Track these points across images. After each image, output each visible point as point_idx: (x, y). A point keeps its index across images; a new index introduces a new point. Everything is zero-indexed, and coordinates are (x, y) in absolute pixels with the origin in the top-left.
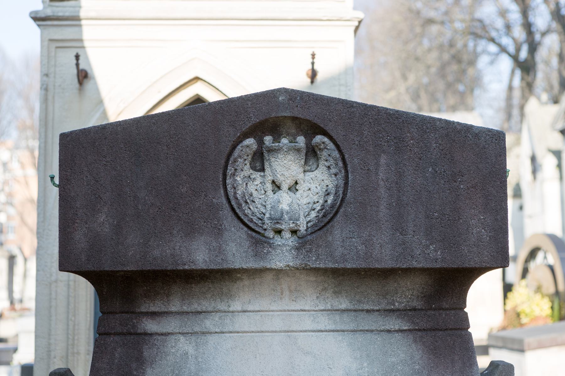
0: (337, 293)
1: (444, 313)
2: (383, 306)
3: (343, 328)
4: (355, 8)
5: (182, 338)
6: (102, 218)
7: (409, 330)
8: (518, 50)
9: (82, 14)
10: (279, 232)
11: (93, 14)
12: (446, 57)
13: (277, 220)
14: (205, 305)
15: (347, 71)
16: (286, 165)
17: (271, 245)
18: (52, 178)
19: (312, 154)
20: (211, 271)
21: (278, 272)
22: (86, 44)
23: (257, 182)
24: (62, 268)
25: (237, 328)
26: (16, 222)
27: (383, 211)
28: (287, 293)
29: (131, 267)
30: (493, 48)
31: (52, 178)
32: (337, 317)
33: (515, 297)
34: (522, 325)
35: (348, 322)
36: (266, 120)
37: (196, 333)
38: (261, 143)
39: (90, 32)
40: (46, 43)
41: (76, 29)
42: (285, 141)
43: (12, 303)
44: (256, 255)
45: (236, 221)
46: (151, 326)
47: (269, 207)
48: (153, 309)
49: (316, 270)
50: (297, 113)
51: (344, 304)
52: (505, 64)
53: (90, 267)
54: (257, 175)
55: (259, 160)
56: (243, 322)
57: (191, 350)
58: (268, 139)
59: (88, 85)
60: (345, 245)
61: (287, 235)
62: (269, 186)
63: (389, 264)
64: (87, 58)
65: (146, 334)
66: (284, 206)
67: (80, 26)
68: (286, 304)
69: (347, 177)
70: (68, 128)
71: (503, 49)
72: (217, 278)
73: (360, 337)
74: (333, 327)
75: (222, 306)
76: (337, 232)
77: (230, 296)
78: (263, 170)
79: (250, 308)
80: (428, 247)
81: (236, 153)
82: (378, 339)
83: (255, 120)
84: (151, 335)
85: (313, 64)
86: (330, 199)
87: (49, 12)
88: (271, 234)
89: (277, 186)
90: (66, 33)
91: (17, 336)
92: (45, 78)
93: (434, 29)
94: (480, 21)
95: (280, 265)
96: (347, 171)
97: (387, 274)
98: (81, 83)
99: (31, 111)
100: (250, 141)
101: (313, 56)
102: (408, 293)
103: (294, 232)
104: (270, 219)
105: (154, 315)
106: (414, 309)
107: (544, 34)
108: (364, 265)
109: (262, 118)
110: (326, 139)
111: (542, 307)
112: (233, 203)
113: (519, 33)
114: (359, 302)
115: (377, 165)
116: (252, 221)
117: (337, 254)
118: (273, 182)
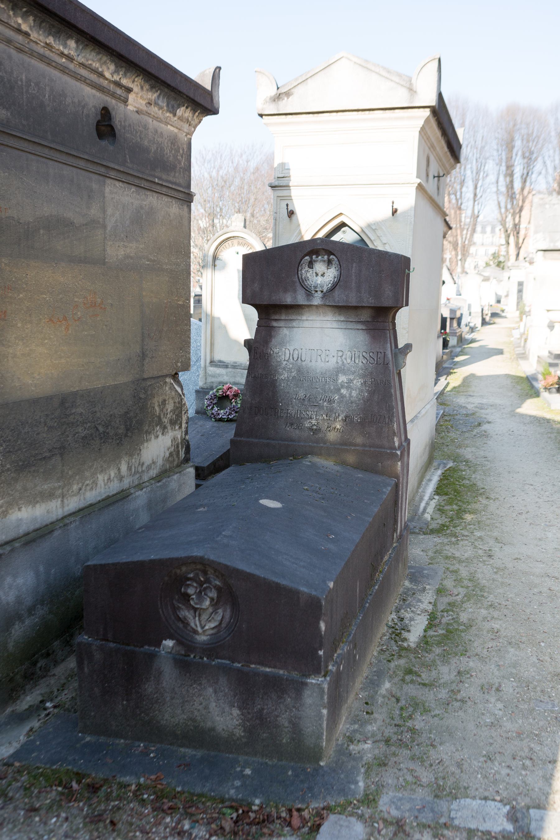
0: (340, 314)
1: (379, 323)
2: (356, 320)
5: (285, 329)
6: (256, 285)
9: (291, 184)
10: (317, 291)
11: (296, 184)
13: (315, 287)
14: (293, 317)
16: (320, 267)
17: (313, 296)
20: (293, 305)
22: (293, 198)
25: (304, 326)
27: (353, 285)
28: (322, 314)
35: (343, 325)
36: (313, 250)
38: (311, 258)
39: (294, 192)
40: (276, 198)
41: (288, 191)
42: (320, 257)
44: (308, 300)
45: (301, 287)
46: (275, 324)
48: (276, 318)
50: (324, 247)
51: (342, 319)
53: (252, 303)
54: (310, 270)
55: (311, 265)
56: (306, 324)
57: (288, 333)
59: (294, 217)
60: (339, 297)
61: (319, 293)
62: (314, 274)
63: (354, 304)
66: (319, 282)
67: (290, 189)
72: (295, 308)
75: (299, 318)
76: (336, 292)
77: (302, 314)
79: (309, 319)
80: (369, 298)
82: (353, 332)
83: (309, 250)
86: (336, 279)
87: (276, 184)
88: (313, 292)
89: (317, 275)
92: (275, 214)
95: (316, 303)
97: (356, 308)
100: (307, 258)
101: (393, 203)
103: (322, 292)
105: (276, 320)
106: (368, 322)
109: (311, 249)
110: (334, 257)
115: (352, 267)
117: (336, 300)
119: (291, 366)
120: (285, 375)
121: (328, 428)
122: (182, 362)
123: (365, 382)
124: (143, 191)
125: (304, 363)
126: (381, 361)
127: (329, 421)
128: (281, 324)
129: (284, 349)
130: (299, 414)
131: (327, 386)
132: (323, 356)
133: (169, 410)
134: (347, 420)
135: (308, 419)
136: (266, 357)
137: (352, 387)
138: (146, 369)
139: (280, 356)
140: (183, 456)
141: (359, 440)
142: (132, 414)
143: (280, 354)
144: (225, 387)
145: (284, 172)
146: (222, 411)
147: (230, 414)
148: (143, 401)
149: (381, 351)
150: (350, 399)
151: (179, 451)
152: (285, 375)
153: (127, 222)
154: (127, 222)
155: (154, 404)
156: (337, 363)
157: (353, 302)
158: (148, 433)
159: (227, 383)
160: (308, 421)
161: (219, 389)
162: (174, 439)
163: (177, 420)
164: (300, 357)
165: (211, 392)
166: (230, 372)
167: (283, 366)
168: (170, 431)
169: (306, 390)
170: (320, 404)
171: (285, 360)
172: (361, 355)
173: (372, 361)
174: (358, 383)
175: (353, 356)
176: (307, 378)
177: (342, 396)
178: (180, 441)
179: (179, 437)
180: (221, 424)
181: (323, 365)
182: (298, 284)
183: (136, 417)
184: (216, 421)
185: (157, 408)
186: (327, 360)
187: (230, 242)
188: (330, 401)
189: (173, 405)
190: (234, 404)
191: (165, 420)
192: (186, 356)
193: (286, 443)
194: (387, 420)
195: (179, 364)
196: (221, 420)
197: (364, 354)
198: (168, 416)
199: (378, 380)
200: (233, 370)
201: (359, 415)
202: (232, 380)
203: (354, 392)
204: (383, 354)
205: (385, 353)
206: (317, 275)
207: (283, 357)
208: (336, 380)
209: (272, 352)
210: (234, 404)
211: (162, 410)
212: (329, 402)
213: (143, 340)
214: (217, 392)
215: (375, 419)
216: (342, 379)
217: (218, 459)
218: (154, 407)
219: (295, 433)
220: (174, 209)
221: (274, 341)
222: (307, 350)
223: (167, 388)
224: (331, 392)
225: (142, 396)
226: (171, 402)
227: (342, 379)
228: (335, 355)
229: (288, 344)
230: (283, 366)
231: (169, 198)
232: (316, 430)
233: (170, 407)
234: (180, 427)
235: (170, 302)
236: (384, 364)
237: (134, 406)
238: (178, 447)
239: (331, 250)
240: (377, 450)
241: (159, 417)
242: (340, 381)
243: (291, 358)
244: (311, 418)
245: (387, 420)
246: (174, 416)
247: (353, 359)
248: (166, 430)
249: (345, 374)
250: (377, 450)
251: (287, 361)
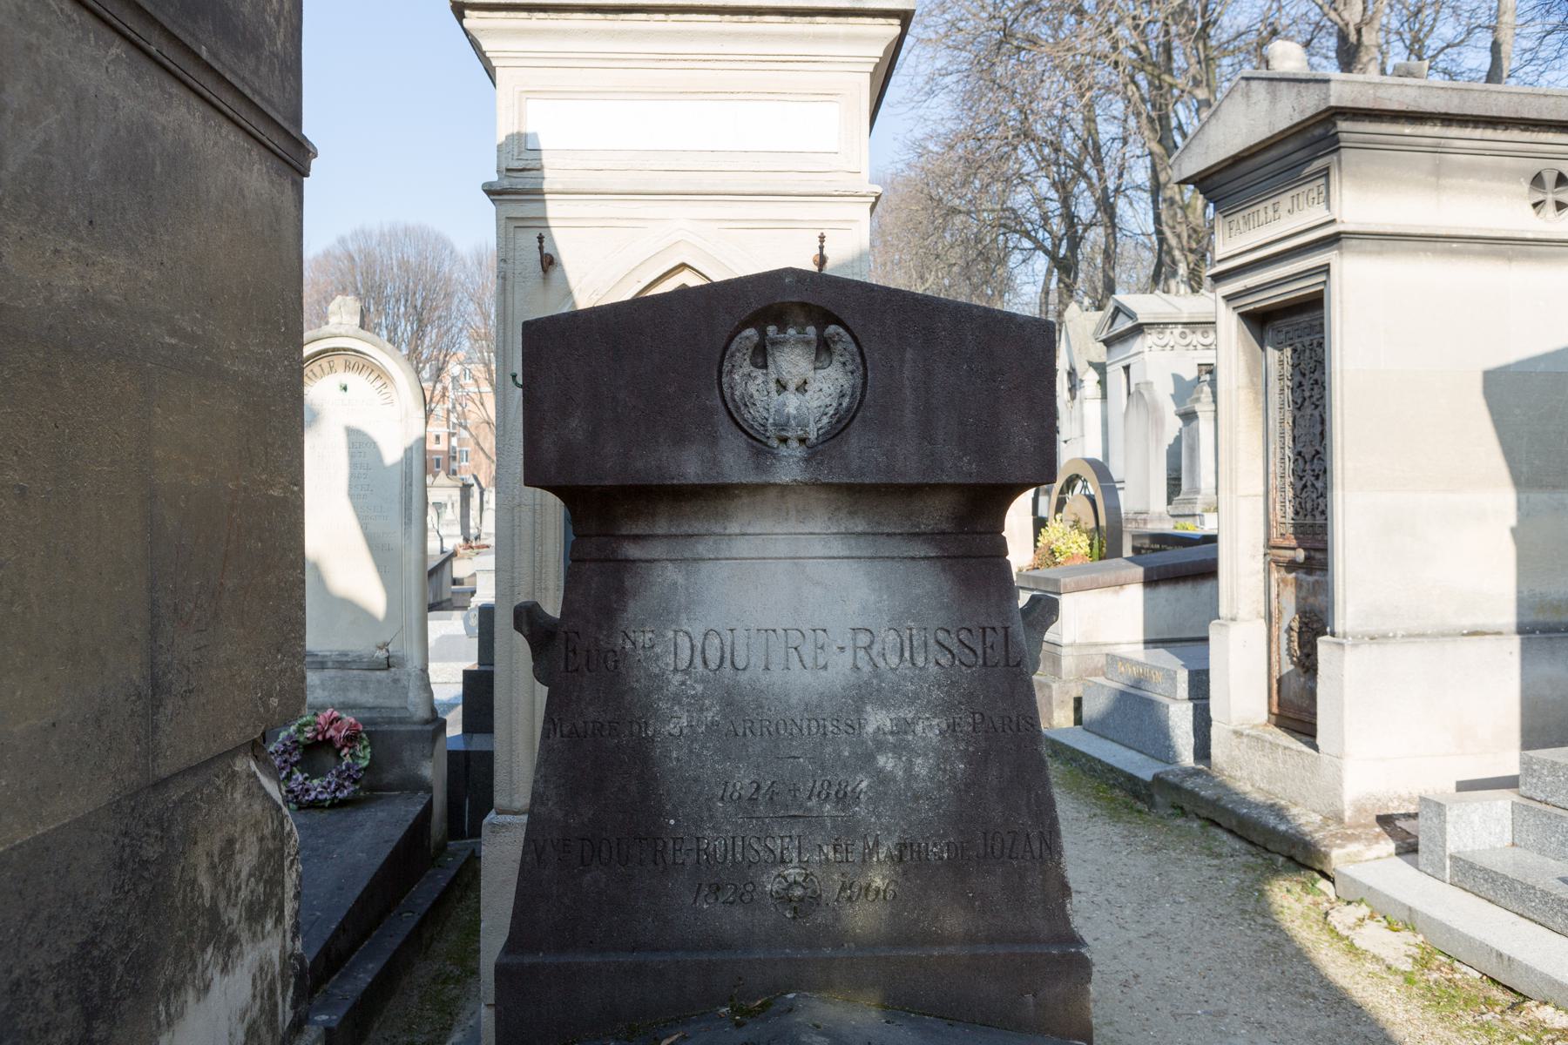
0: (852, 514)
2: (906, 529)
3: (859, 553)
4: (871, 182)
7: (937, 557)
8: (1057, 246)
9: (546, 186)
10: (784, 440)
11: (558, 187)
12: (972, 254)
13: (782, 426)
14: (698, 527)
15: (861, 257)
16: (793, 362)
17: (775, 456)
18: (514, 377)
19: (823, 348)
20: (704, 487)
21: (784, 488)
22: (551, 223)
23: (759, 381)
24: (529, 482)
26: (470, 447)
29: (608, 482)
30: (1027, 244)
31: (514, 377)
32: (853, 542)
33: (1048, 535)
34: (1056, 564)
37: (686, 560)
38: (763, 334)
39: (555, 209)
42: (792, 331)
43: (467, 540)
44: (758, 468)
45: (734, 428)
46: (633, 551)
47: (772, 411)
48: (635, 531)
49: (828, 486)
52: (1041, 262)
53: (561, 481)
54: (758, 373)
55: (761, 356)
56: (741, 547)
57: (680, 580)
58: (772, 330)
59: (554, 274)
60: (863, 457)
61: (794, 444)
62: (773, 386)
63: (914, 478)
64: (552, 240)
65: (627, 561)
66: (791, 410)
68: (792, 526)
69: (865, 376)
70: (532, 316)
71: (1039, 246)
72: (712, 496)
73: (879, 565)
74: (847, 553)
75: (718, 529)
76: (853, 441)
77: (727, 517)
78: (765, 366)
79: (751, 530)
80: (960, 458)
81: (734, 346)
82: (901, 567)
83: (756, 306)
84: (634, 561)
85: (821, 248)
87: (506, 184)
88: (775, 443)
89: (782, 386)
90: (528, 210)
91: (474, 575)
93: (958, 220)
94: (1014, 211)
95: (786, 479)
96: (865, 369)
97: (911, 491)
98: (545, 270)
99: (486, 317)
101: (822, 238)
102: (935, 514)
103: (802, 441)
104: (774, 424)
105: (636, 538)
106: (943, 533)
107: (1087, 227)
108: (884, 480)
109: (764, 304)
110: (841, 330)
111: (1079, 544)
112: (730, 405)
113: (1057, 225)
114: (879, 523)
116: (752, 427)
117: (854, 466)
118: (778, 381)
119: (699, 688)
120: (680, 721)
121: (843, 889)
122: (280, 694)
123: (952, 727)
124: (153, 75)
125: (743, 677)
126: (997, 656)
127: (845, 868)
128: (657, 550)
129: (671, 634)
130: (738, 849)
131: (829, 749)
132: (808, 651)
133: (244, 875)
134: (907, 856)
135: (774, 864)
136: (611, 664)
137: (912, 748)
138: (164, 742)
139: (658, 657)
140: (289, 1016)
141: (953, 921)
142: (110, 941)
143: (658, 650)
144: (321, 720)
145: (524, 156)
146: (316, 782)
147: (340, 787)
148: (154, 869)
149: (997, 625)
150: (909, 788)
151: (276, 1005)
152: (680, 721)
153: (95, 167)
154: (95, 167)
155: (195, 867)
156: (856, 668)
157: (911, 473)
158: (175, 988)
159: (324, 708)
160: (775, 873)
161: (305, 725)
162: (261, 969)
163: (269, 896)
164: (728, 655)
165: (283, 735)
166: (332, 678)
167: (672, 689)
168: (247, 947)
169: (758, 767)
170: (810, 810)
171: (676, 670)
172: (932, 642)
173: (969, 658)
174: (929, 730)
175: (907, 643)
176: (757, 725)
177: (882, 779)
178: (278, 968)
179: (276, 953)
180: (318, 815)
181: (808, 677)
182: (722, 416)
183: (127, 946)
184: (300, 809)
185: (205, 881)
186: (821, 662)
187: (324, 362)
188: (844, 799)
189: (255, 850)
190: (348, 759)
191: (233, 914)
192: (292, 669)
193: (704, 957)
194: (1036, 845)
195: (274, 701)
196: (315, 805)
197: (941, 635)
198: (243, 894)
199: (995, 719)
200: (340, 673)
201: (944, 836)
202: (338, 698)
203: (919, 761)
204: (1001, 632)
205: (1006, 629)
206: (782, 386)
207: (670, 659)
208: (856, 727)
209: (629, 646)
210: (348, 759)
211: (220, 882)
212: (838, 800)
213: (154, 633)
214: (300, 731)
215: (998, 846)
216: (877, 720)
217: (335, 936)
218: (195, 880)
219: (728, 918)
220: (257, 176)
221: (634, 609)
222: (753, 632)
223: (238, 796)
224: (845, 766)
225: (151, 852)
226: (251, 838)
227: (877, 720)
228: (848, 643)
229: (683, 616)
230: (672, 689)
231: (241, 134)
232: (801, 899)
233: (247, 859)
234: (279, 920)
235: (246, 489)
236: (1007, 665)
237: (117, 902)
238: (272, 991)
239: (829, 307)
240: (1017, 949)
241: (214, 914)
242: (870, 729)
243: (698, 661)
244: (783, 861)
245: (1036, 845)
246: (261, 888)
247: (907, 655)
248: (235, 951)
249: (884, 704)
250: (1017, 949)
251: (686, 671)
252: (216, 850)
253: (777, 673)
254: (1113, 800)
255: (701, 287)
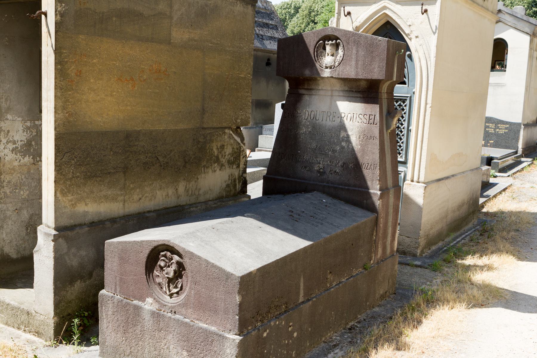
46: (302, 91)
125: (317, 122)
127: (331, 166)
133: (227, 153)
177: (343, 148)
195: (239, 121)
208: (338, 136)
218: (212, 149)
242: (341, 136)
251: (306, 119)
252: (219, 146)
253: (324, 122)
254: (79, 74)
255: (291, 37)
